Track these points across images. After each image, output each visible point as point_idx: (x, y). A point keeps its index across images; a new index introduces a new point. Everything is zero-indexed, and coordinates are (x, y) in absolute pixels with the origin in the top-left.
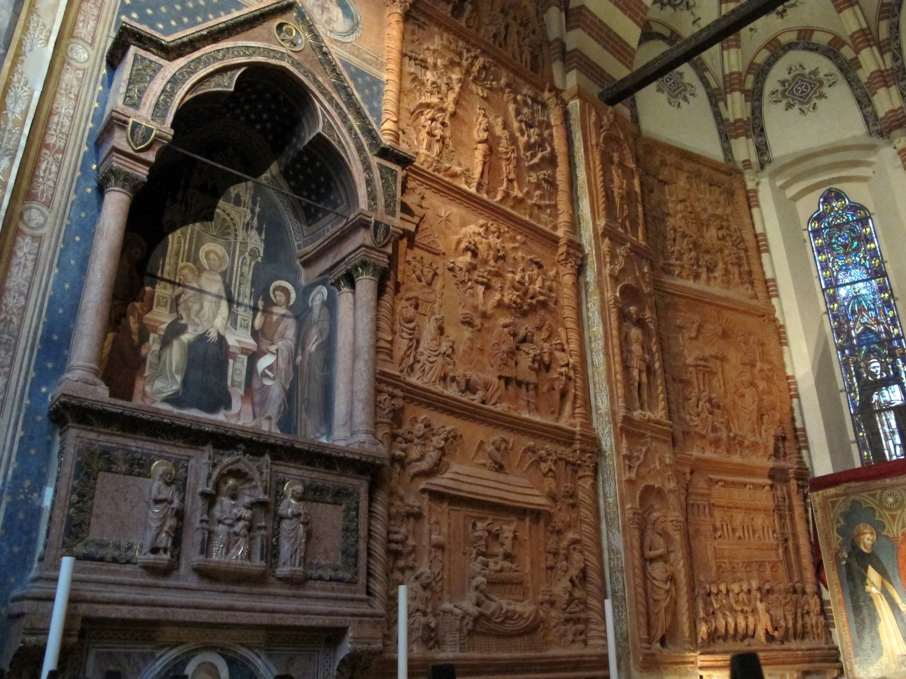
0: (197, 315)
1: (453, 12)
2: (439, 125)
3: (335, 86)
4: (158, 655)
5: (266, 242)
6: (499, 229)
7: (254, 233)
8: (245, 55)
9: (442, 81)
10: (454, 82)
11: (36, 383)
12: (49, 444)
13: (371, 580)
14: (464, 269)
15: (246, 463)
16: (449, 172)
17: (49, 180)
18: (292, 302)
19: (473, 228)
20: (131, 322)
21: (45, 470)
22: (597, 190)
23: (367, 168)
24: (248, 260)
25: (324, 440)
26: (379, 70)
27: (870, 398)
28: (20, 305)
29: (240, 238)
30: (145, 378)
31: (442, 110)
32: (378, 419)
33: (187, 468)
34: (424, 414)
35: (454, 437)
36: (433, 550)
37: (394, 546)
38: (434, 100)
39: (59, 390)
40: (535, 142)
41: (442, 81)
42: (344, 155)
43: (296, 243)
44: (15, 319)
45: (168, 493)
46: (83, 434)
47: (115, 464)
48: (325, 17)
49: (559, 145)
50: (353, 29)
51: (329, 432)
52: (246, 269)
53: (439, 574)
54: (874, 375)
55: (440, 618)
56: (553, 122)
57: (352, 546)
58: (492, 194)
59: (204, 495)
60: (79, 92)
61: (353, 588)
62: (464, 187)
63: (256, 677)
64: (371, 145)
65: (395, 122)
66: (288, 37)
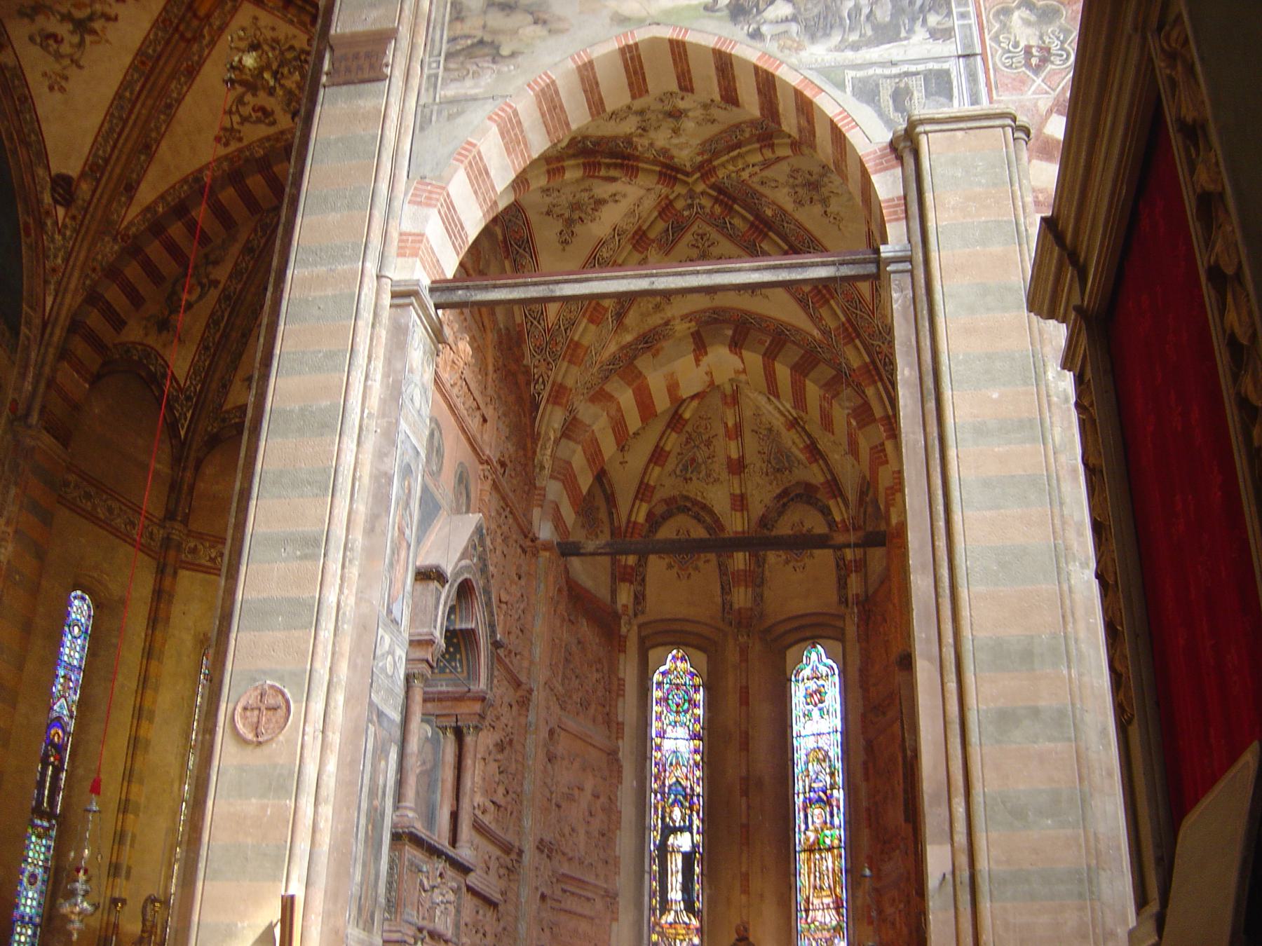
27: (667, 839)
54: (674, 821)
63: (754, 945)
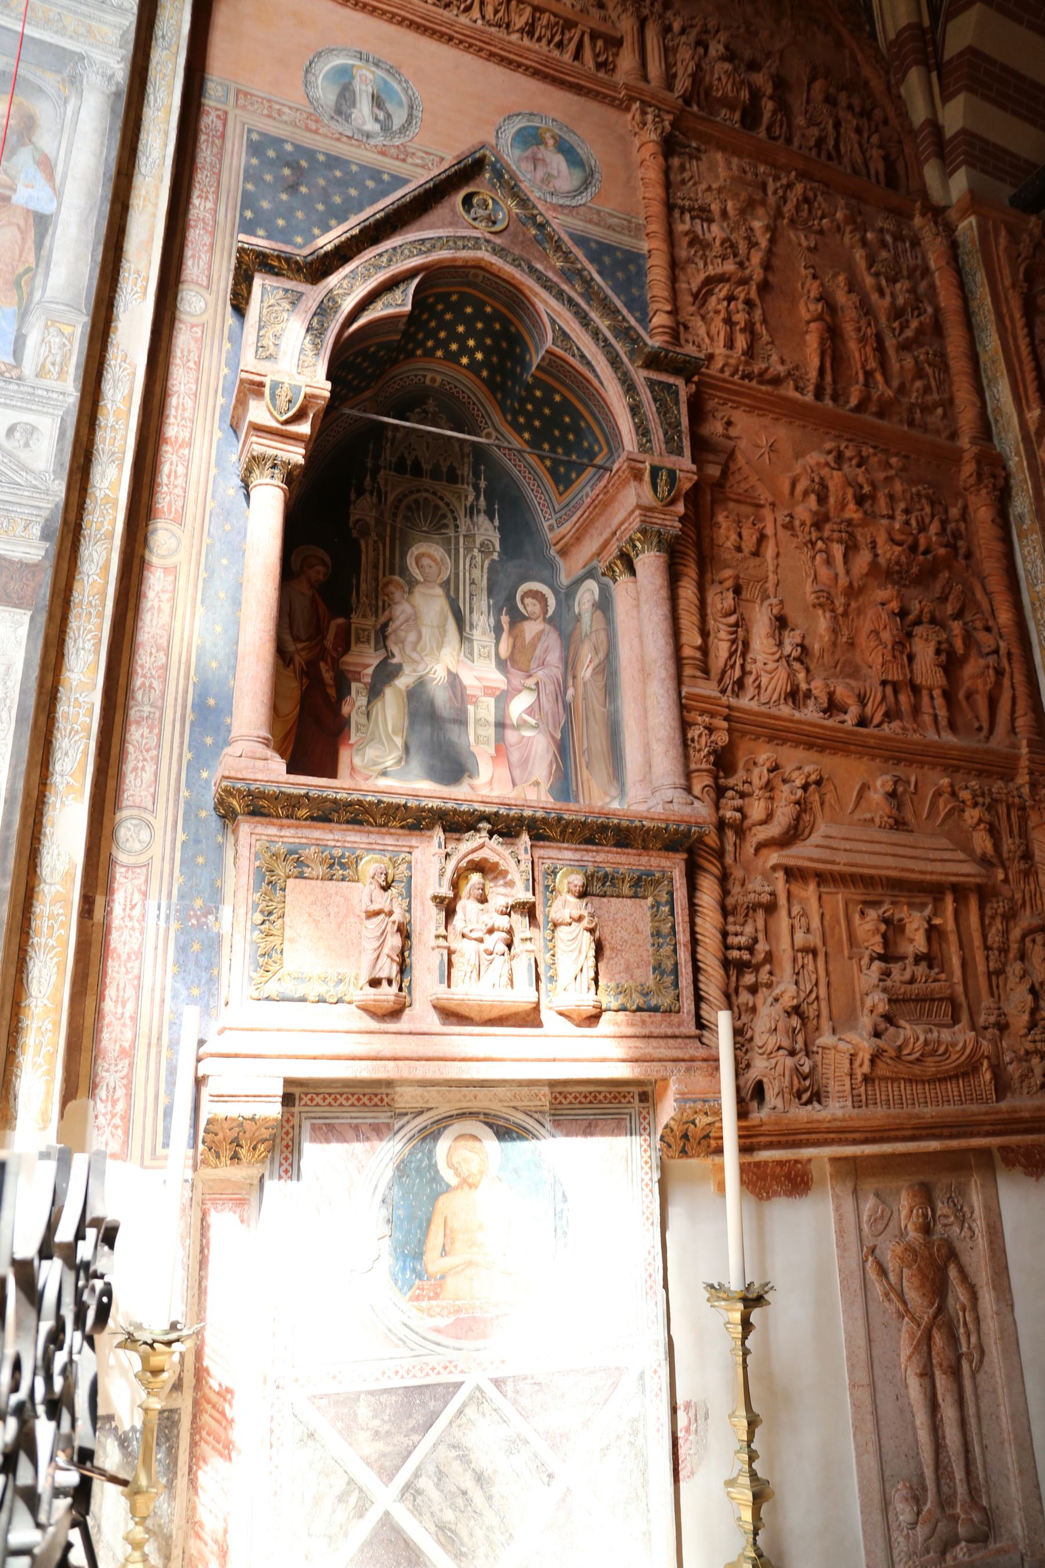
0: (414, 649)
1: (743, 121)
2: (741, 306)
3: (563, 273)
4: (396, 1127)
5: (501, 529)
6: (860, 452)
7: (482, 519)
8: (421, 252)
9: (739, 238)
10: (758, 233)
11: (194, 767)
12: (221, 847)
13: (703, 1005)
14: (808, 523)
15: (494, 850)
16: (768, 376)
17: (175, 487)
18: (550, 613)
19: (814, 458)
20: (323, 671)
21: (219, 883)
22: (1021, 362)
23: (630, 388)
24: (479, 559)
25: (615, 805)
26: (635, 237)
28: (159, 664)
29: (463, 530)
30: (352, 745)
31: (744, 282)
32: (693, 767)
33: (410, 863)
34: (765, 755)
35: (819, 783)
36: (799, 955)
37: (735, 954)
38: (729, 267)
39: (221, 771)
40: (905, 303)
41: (739, 238)
42: (590, 375)
43: (546, 524)
44: (155, 684)
45: (382, 900)
46: (260, 829)
47: (308, 866)
48: (540, 173)
49: (948, 299)
50: (586, 184)
51: (622, 792)
52: (476, 573)
53: (811, 992)
55: (818, 1058)
56: (932, 265)
57: (668, 957)
58: (842, 399)
59: (438, 900)
60: (199, 357)
61: (675, 1018)
62: (793, 394)
64: (632, 354)
65: (669, 313)
66: (481, 212)
